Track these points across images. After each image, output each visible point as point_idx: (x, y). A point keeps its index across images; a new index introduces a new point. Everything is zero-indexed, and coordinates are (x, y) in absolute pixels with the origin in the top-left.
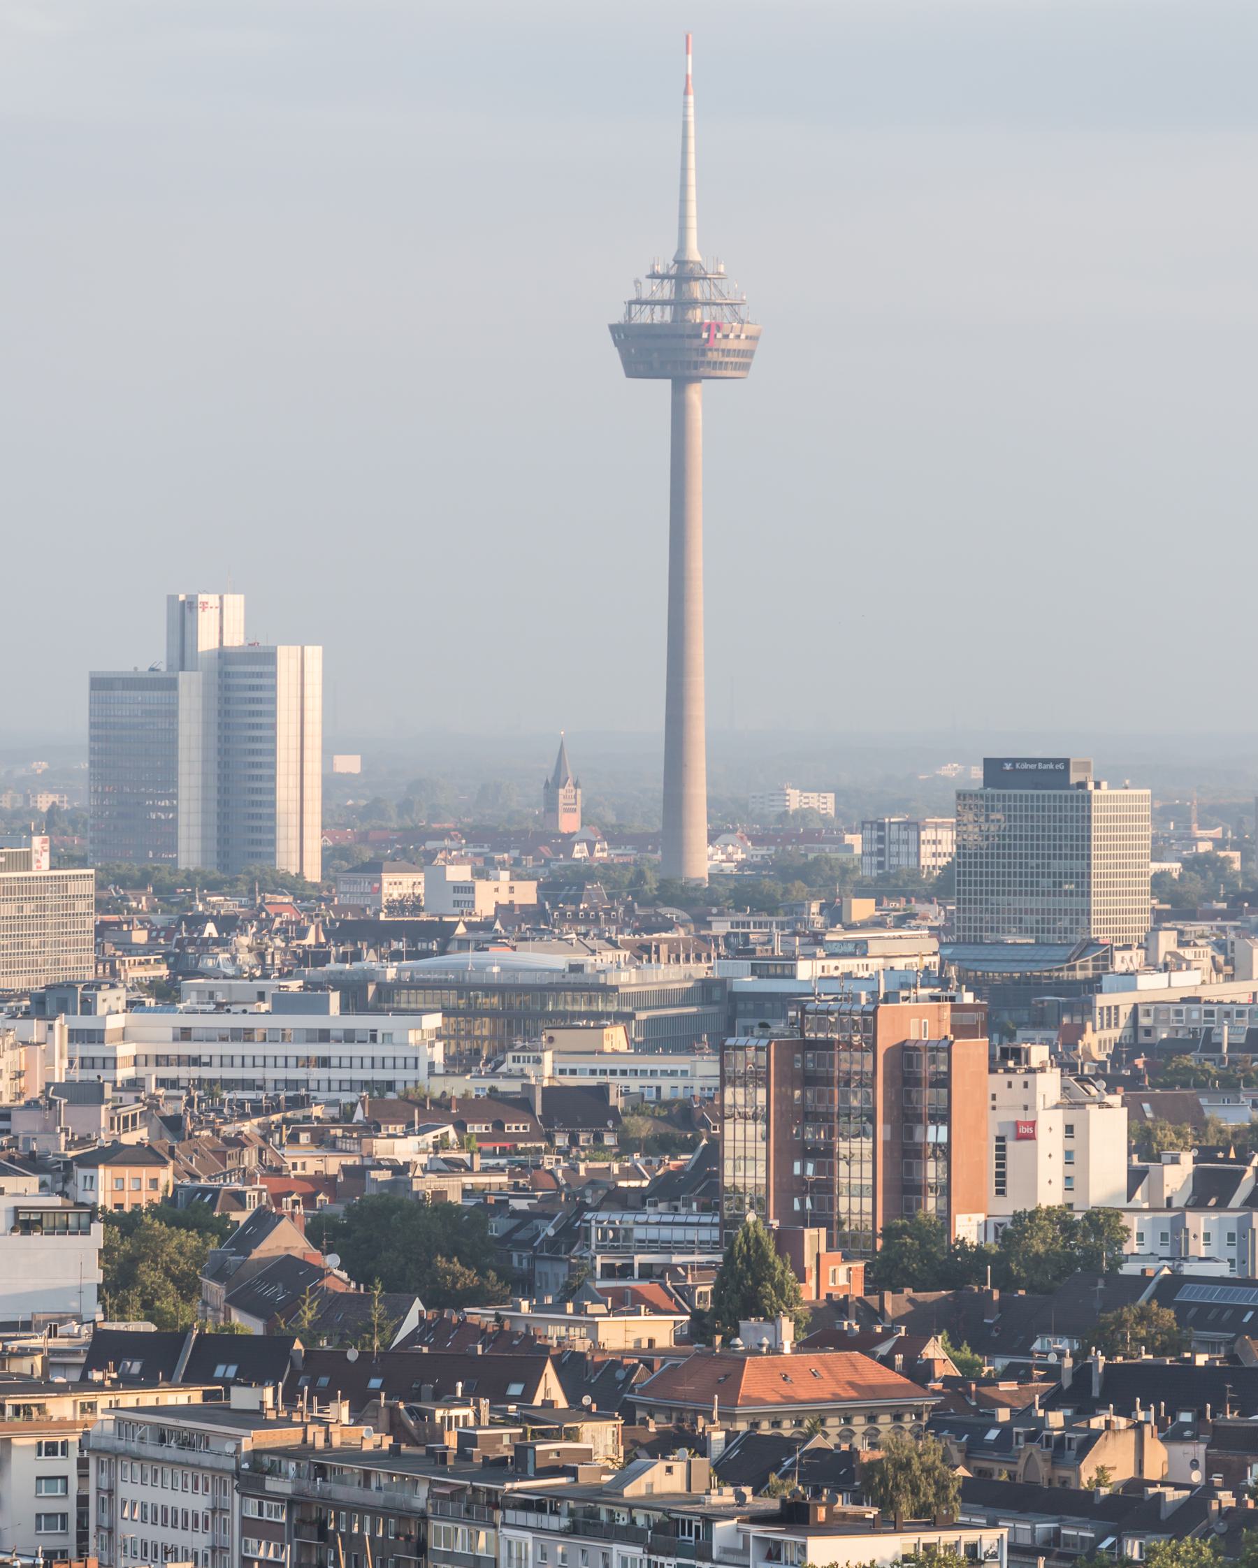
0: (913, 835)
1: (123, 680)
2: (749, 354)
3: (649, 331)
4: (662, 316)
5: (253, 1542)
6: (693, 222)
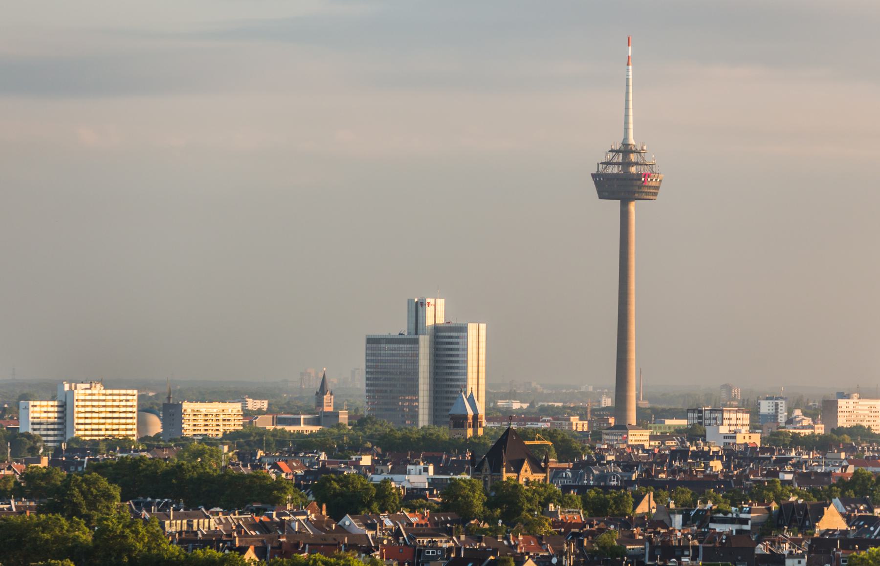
0: (718, 415)
1: (387, 339)
2: (657, 188)
4: (614, 170)
6: (631, 126)
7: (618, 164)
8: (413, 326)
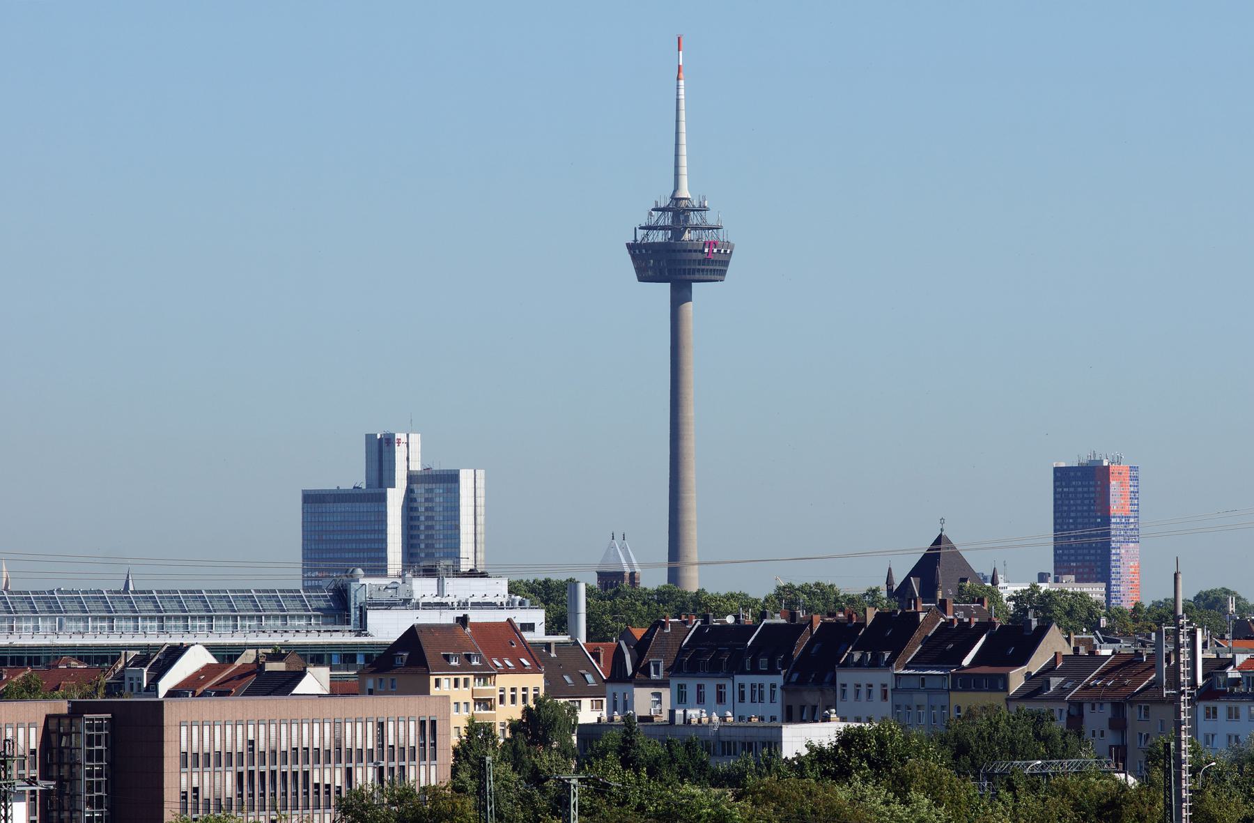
3: (654, 248)
4: (659, 237)
5: (398, 662)
6: (684, 171)
7: (663, 228)
8: (375, 474)
